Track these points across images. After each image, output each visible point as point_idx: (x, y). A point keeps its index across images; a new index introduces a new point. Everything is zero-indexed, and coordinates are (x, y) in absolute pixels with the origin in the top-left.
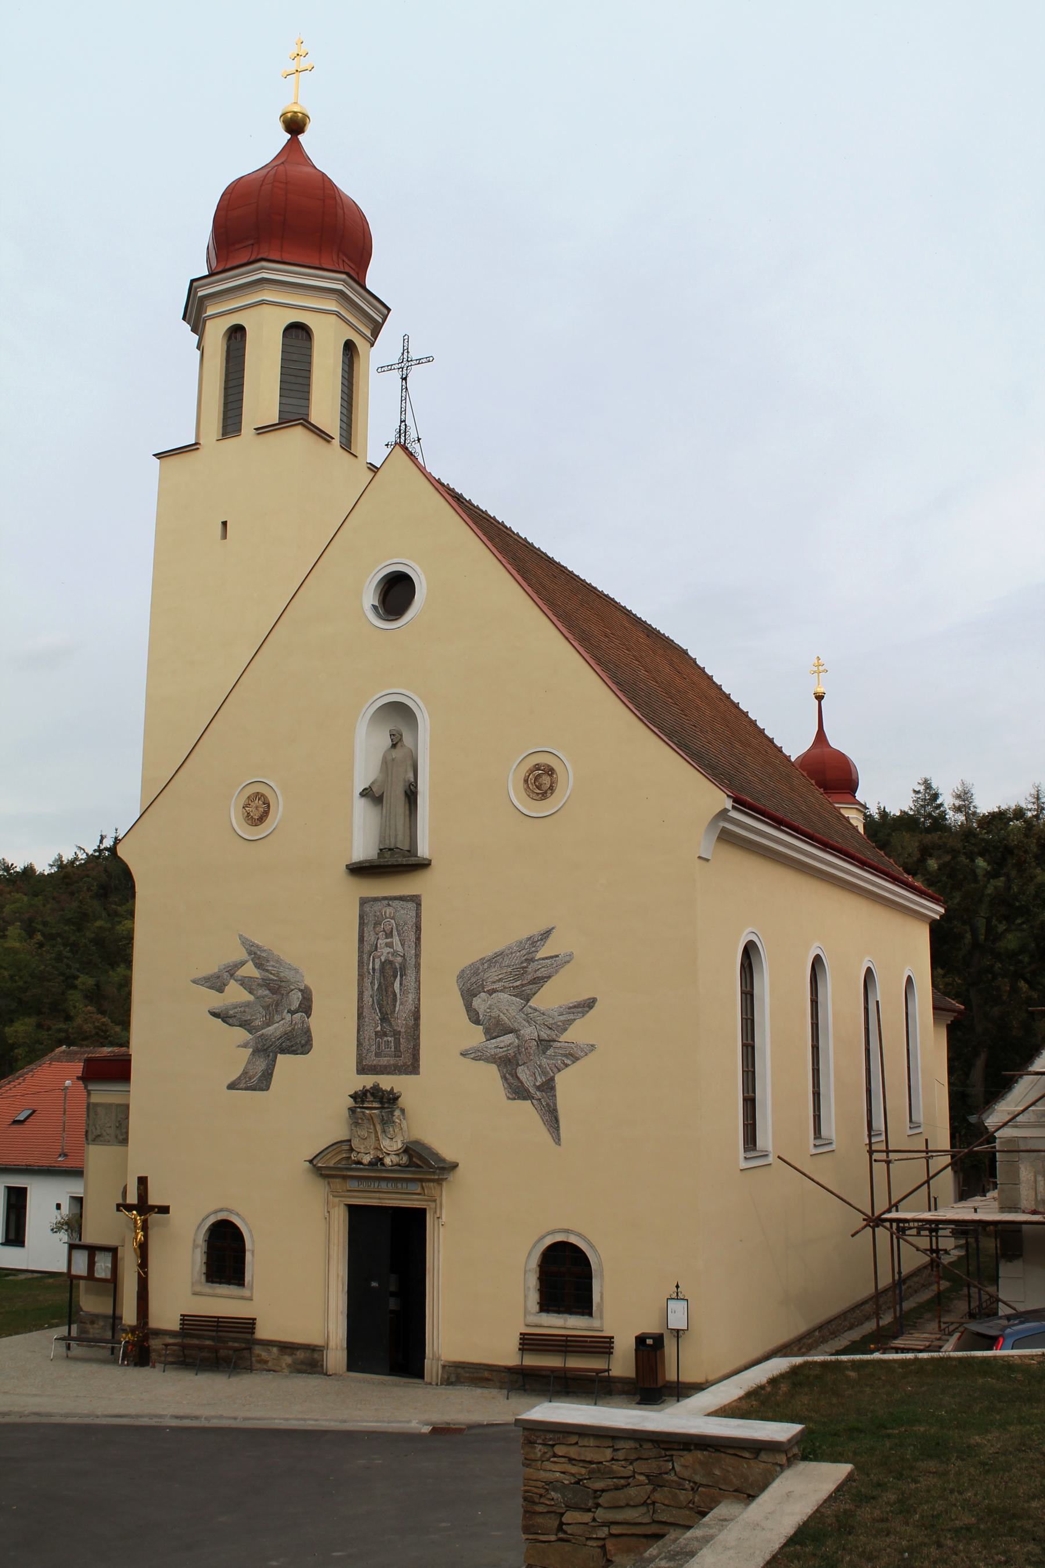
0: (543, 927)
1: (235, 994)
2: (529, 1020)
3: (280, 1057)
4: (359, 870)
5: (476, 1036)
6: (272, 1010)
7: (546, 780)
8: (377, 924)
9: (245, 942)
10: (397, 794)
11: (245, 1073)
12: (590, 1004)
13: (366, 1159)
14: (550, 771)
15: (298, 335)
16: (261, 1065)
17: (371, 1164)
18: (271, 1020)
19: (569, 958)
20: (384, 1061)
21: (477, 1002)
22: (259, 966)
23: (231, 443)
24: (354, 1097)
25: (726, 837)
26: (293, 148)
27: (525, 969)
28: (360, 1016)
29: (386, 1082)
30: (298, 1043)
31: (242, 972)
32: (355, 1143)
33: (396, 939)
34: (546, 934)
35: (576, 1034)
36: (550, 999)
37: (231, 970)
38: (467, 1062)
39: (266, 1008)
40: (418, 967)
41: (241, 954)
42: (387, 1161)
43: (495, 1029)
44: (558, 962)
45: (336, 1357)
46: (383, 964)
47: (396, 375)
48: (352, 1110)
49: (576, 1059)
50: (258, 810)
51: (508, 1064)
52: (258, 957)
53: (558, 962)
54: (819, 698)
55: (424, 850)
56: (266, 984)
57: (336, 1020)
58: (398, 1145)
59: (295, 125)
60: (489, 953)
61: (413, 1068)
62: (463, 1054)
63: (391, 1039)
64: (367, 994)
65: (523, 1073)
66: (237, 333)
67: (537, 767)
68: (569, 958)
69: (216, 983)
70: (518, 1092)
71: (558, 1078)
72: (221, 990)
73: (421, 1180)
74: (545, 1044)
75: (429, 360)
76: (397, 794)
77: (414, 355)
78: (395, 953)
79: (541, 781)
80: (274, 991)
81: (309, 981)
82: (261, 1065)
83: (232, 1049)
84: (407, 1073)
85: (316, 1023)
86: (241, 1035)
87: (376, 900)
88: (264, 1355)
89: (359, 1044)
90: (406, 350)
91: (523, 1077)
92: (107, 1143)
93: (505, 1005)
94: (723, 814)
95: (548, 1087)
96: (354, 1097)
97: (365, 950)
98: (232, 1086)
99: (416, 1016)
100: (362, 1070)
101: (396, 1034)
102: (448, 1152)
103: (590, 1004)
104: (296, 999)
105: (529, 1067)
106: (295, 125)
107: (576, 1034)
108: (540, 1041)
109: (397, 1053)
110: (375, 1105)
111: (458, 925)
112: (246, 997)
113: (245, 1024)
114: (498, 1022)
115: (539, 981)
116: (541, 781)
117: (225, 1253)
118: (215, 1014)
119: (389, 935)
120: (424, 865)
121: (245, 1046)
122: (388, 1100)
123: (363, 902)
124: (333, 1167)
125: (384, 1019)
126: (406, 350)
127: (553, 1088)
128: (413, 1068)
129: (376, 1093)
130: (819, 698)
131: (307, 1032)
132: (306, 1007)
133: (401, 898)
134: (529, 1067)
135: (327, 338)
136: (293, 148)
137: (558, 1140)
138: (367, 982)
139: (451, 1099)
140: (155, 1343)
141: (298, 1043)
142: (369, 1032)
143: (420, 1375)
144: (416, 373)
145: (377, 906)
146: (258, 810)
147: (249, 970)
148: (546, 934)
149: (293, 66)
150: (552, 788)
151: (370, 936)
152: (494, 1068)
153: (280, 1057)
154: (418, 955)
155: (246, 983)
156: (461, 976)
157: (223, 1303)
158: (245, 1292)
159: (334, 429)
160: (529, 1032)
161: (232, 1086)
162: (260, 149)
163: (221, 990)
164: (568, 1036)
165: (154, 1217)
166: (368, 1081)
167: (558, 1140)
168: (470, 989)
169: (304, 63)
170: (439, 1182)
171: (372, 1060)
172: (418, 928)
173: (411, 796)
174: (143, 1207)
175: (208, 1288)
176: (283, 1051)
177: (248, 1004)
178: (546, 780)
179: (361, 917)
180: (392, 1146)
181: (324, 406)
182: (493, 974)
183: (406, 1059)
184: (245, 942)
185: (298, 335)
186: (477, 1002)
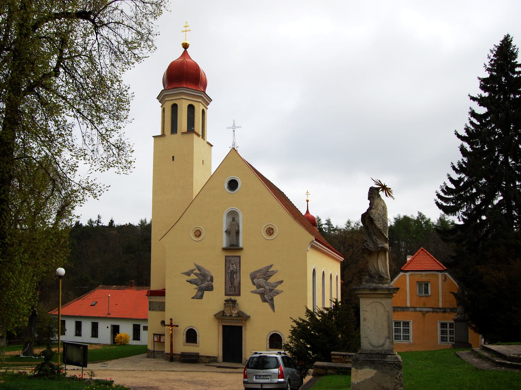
0: (271, 264)
1: (193, 277)
2: (267, 285)
3: (205, 292)
4: (224, 249)
5: (254, 288)
6: (203, 281)
7: (271, 231)
8: (230, 262)
9: (195, 265)
10: (233, 232)
11: (196, 295)
12: (282, 282)
13: (228, 315)
14: (272, 229)
15: (191, 108)
16: (200, 293)
17: (229, 316)
18: (203, 283)
19: (277, 272)
20: (232, 293)
21: (254, 281)
22: (199, 270)
23: (174, 136)
24: (225, 301)
25: (313, 247)
26: (185, 54)
27: (266, 273)
28: (225, 283)
29: (233, 298)
30: (210, 288)
31: (194, 272)
32: (225, 311)
33: (234, 266)
34: (271, 266)
35: (279, 288)
36: (272, 280)
37: (192, 271)
38: (252, 294)
39: (201, 280)
40: (240, 272)
41: (194, 267)
42: (233, 315)
43: (259, 286)
44: (274, 272)
45: (220, 358)
46: (231, 271)
47: (232, 130)
48: (225, 304)
49: (278, 294)
50: (198, 234)
51: (262, 295)
52: (199, 268)
53: (274, 272)
54: (308, 201)
55: (241, 245)
56: (201, 274)
57: (219, 283)
58: (236, 312)
59: (186, 46)
60: (257, 269)
61: (239, 295)
62: (251, 292)
63: (233, 288)
64: (227, 278)
65: (266, 297)
66: (175, 107)
67: (269, 228)
68: (277, 272)
69: (188, 274)
70: (265, 300)
71: (274, 298)
72: (189, 276)
73: (242, 320)
74: (271, 290)
75: (240, 127)
76: (233, 232)
77: (236, 125)
78: (234, 269)
79: (270, 231)
80: (203, 277)
81: (213, 274)
82: (200, 293)
83: (193, 289)
84: (237, 296)
85: (214, 284)
86: (195, 286)
87: (229, 256)
88: (202, 359)
89: (225, 289)
90: (234, 124)
91: (266, 297)
92: (156, 311)
93: (262, 281)
94: (313, 241)
95: (272, 300)
96: (225, 301)
97: (227, 268)
98: (193, 298)
99: (240, 283)
100: (226, 295)
101: (235, 287)
102: (248, 313)
103: (282, 282)
104: (209, 278)
105: (268, 295)
106: (186, 46)
107: (279, 288)
108: (270, 289)
109: (235, 291)
110: (231, 303)
111: (249, 264)
112: (196, 277)
113: (196, 284)
114: (260, 285)
115: (270, 276)
116: (270, 231)
117: (191, 336)
118: (188, 281)
119: (233, 264)
120: (241, 249)
121: (196, 289)
122: (234, 302)
123: (226, 257)
124: (220, 316)
125: (231, 284)
126: (234, 124)
127: (273, 300)
128: (239, 295)
129: (231, 300)
130: (308, 201)
131: (212, 286)
132: (212, 280)
133: (236, 256)
134: (268, 295)
135: (199, 108)
136: (185, 54)
137: (274, 311)
138: (227, 275)
139: (249, 301)
140: (174, 357)
141: (210, 288)
142: (228, 286)
143: (241, 363)
144: (236, 130)
145: (229, 258)
146: (198, 234)
147: (197, 271)
148: (271, 266)
149: (184, 29)
150: (273, 233)
151: (228, 265)
152: (259, 295)
153: (205, 292)
154: (240, 269)
155: (195, 274)
156: (251, 275)
157: (191, 349)
158: (197, 345)
159: (201, 134)
160: (267, 287)
161: (193, 298)
162: (176, 54)
163: (189, 276)
164: (276, 289)
165: (174, 328)
166: (228, 297)
167: (274, 311)
168: (253, 277)
169: (188, 29)
170: (246, 320)
171: (228, 293)
172: (240, 263)
173: (238, 233)
174: (171, 325)
175: (187, 344)
176: (206, 290)
177: (196, 279)
178: (271, 231)
179: (226, 260)
180: (235, 312)
181: (198, 128)
182: (258, 274)
183: (237, 292)
184: (195, 265)
185: (191, 108)
186: (254, 281)
